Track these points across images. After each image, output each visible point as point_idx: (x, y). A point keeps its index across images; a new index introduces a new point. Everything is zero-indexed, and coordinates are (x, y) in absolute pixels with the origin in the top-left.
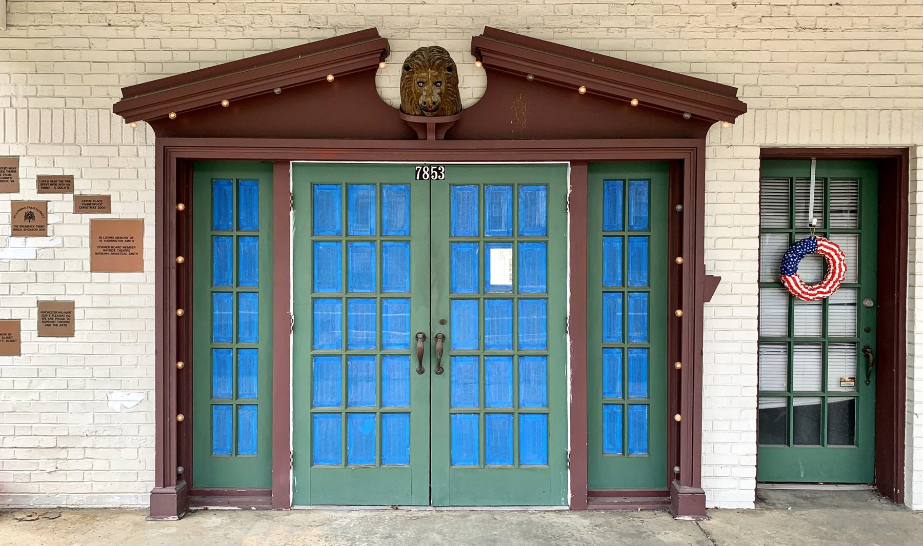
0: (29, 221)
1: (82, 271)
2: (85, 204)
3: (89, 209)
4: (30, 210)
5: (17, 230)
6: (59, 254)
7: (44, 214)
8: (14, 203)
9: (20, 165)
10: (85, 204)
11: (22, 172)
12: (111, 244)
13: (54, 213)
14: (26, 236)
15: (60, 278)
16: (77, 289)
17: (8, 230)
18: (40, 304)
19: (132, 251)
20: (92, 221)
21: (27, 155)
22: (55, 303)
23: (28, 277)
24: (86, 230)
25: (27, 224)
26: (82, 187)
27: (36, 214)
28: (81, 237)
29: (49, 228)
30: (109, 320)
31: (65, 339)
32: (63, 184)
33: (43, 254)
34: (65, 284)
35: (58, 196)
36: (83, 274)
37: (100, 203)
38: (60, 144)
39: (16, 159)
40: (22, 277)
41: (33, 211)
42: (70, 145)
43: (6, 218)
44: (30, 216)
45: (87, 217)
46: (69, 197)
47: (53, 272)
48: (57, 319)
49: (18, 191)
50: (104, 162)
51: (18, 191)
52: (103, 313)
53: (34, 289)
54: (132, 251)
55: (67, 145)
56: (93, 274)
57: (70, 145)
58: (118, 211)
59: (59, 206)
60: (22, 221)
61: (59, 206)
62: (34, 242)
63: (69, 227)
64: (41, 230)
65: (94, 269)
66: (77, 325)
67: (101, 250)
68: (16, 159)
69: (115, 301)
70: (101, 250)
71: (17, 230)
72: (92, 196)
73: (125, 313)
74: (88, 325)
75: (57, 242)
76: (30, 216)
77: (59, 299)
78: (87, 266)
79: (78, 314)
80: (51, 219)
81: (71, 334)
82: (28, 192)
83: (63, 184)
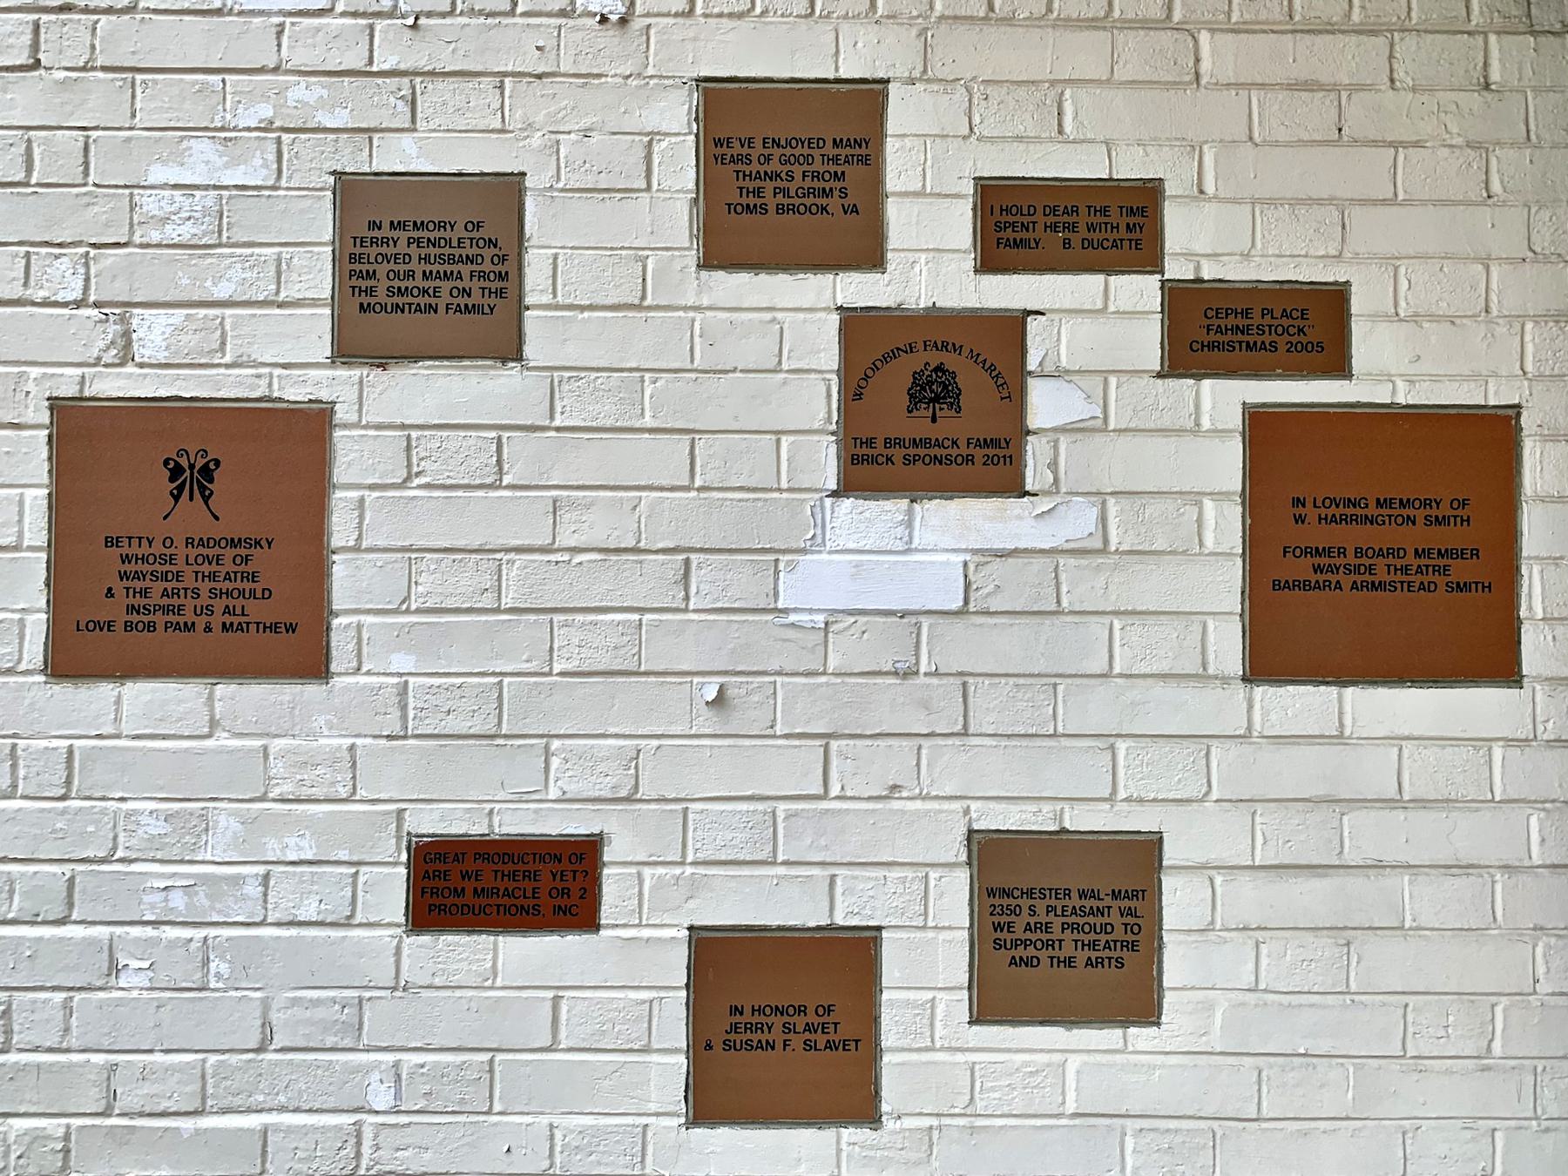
0: (933, 412)
1: (1202, 677)
2: (1216, 329)
3: (1241, 355)
4: (935, 358)
5: (869, 465)
6: (1082, 586)
7: (1010, 382)
8: (857, 326)
9: (892, 125)
10: (1216, 329)
11: (900, 166)
12: (1352, 536)
13: (1059, 374)
14: (917, 490)
15: (1092, 709)
16: (1172, 773)
17: (824, 462)
18: (990, 853)
19: (1461, 570)
20: (1259, 421)
21: (921, 77)
22: (1059, 842)
23: (926, 705)
24: (1226, 464)
25: (919, 426)
26: (1203, 241)
27: (969, 379)
28: (1195, 498)
29: (1035, 453)
30: (1343, 933)
31: (1110, 1036)
32: (1104, 225)
33: (1011, 587)
34: (1108, 740)
35: (1083, 287)
36: (1214, 693)
37: (1305, 326)
38: (1093, 24)
39: (869, 98)
40: (891, 706)
41: (950, 361)
42: (1146, 25)
43: (815, 402)
44: (934, 390)
45: (1224, 400)
46: (1139, 293)
47: (1052, 679)
48: (1070, 927)
49: (992, 1004)
50: (1315, 114)
51: (992, 1004)
52: (1310, 898)
53: (949, 769)
54: (1461, 570)
55: (1129, 25)
56: (1259, 691)
57: (1146, 25)
58: (1391, 366)
59: (1088, 330)
60: (895, 417)
61: (1088, 330)
62: (954, 525)
63: (1143, 456)
64: (989, 460)
65: (1269, 661)
66: (1176, 966)
67: (1302, 568)
68: (869, 98)
69: (1366, 835)
70: (1302, 568)
71: (869, 465)
72: (1255, 290)
73: (1423, 901)
74: (1233, 963)
75: (1077, 523)
76: (934, 390)
77: (1082, 820)
78: (1227, 646)
79: (1180, 902)
80: (1046, 405)
81: (1142, 1007)
82: (929, 262)
83: (1104, 225)
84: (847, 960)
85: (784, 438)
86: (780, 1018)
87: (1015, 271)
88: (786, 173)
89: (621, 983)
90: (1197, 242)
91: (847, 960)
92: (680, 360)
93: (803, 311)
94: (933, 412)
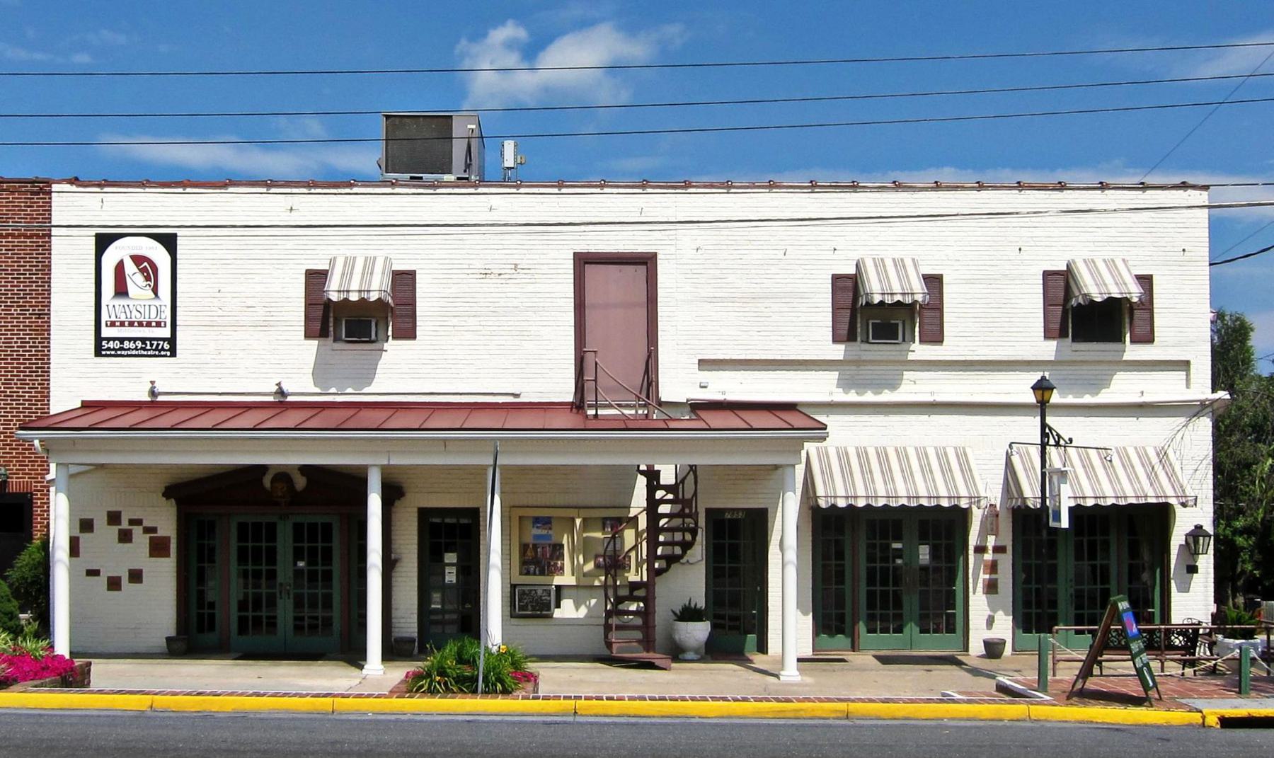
0: (125, 537)
2: (148, 530)
10: (148, 530)
26: (146, 523)
32: (137, 522)
37: (154, 530)
48: (136, 576)
58: (161, 533)
59: (137, 530)
61: (137, 530)
63: (141, 541)
82: (125, 525)
83: (137, 522)
84: (119, 579)
85: (103, 335)
86: (114, 584)
87: (1215, 443)
88: (114, 518)
89: (102, 581)
90: (146, 523)
91: (119, 579)
92: (106, 534)
93: (115, 529)
94: (125, 537)
